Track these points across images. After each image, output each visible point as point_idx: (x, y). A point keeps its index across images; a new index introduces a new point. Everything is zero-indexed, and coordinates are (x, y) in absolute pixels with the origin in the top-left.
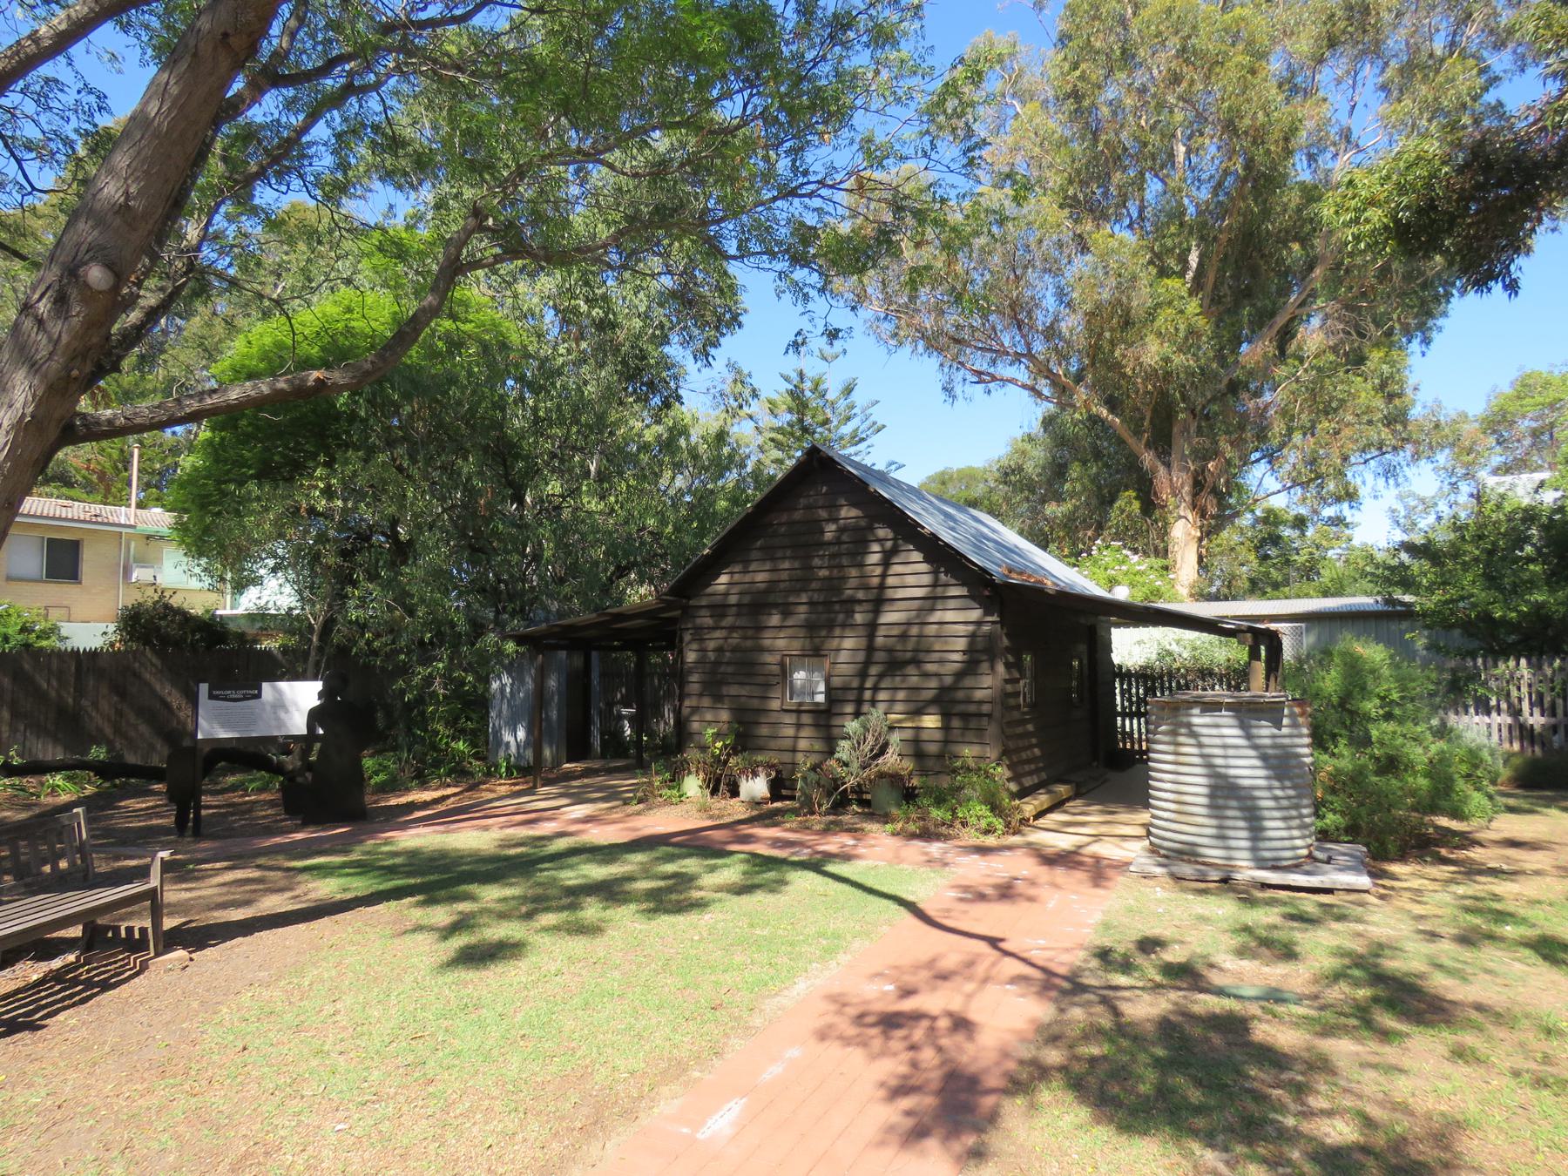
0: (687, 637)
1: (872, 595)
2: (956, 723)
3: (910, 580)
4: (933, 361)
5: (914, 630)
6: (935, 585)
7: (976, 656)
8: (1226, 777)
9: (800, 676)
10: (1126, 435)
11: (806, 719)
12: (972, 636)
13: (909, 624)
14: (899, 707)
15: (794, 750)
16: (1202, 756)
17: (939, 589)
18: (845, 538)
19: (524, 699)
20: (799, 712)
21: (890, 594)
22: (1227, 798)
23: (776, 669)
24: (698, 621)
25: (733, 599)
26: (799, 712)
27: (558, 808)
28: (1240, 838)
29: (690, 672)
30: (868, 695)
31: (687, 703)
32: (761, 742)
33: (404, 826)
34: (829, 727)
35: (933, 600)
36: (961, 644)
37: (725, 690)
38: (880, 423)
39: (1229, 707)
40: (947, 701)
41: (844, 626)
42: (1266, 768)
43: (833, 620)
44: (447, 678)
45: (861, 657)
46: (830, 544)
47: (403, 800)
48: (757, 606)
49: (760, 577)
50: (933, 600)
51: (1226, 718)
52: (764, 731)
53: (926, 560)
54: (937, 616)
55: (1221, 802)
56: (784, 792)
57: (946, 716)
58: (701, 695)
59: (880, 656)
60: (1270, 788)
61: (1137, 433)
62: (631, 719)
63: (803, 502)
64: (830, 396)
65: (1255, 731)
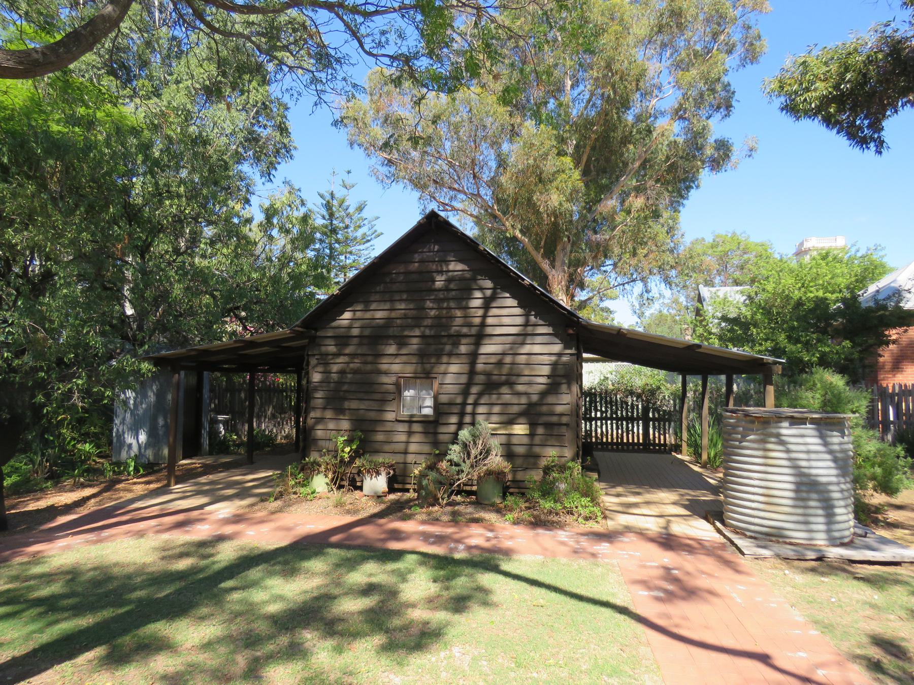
0: (313, 361)
1: (474, 331)
2: (540, 430)
3: (506, 320)
4: (416, 194)
5: (508, 359)
6: (526, 324)
7: (558, 379)
8: (809, 475)
9: (409, 394)
10: (530, 248)
11: (417, 427)
12: (554, 365)
13: (504, 354)
14: (495, 418)
15: (406, 453)
16: (789, 459)
17: (529, 329)
18: (452, 286)
19: (145, 410)
20: (410, 422)
21: (489, 330)
22: (808, 492)
23: (391, 388)
24: (323, 349)
25: (355, 332)
26: (410, 422)
27: (201, 507)
28: (819, 523)
29: (316, 390)
30: (469, 409)
31: (312, 415)
32: (377, 446)
33: (50, 536)
34: (436, 433)
35: (523, 337)
36: (546, 370)
37: (347, 405)
38: (379, 232)
39: (813, 421)
40: (532, 413)
41: (450, 355)
42: (836, 468)
43: (442, 350)
44: (86, 393)
45: (464, 379)
46: (440, 290)
47: (42, 504)
48: (375, 338)
49: (379, 315)
50: (523, 337)
51: (809, 429)
52: (380, 437)
53: (520, 305)
54: (526, 349)
55: (804, 495)
56: (396, 486)
57: (533, 425)
58: (324, 408)
59: (480, 379)
60: (838, 484)
61: (537, 248)
62: (226, 423)
63: (417, 257)
64: (351, 210)
65: (829, 439)
